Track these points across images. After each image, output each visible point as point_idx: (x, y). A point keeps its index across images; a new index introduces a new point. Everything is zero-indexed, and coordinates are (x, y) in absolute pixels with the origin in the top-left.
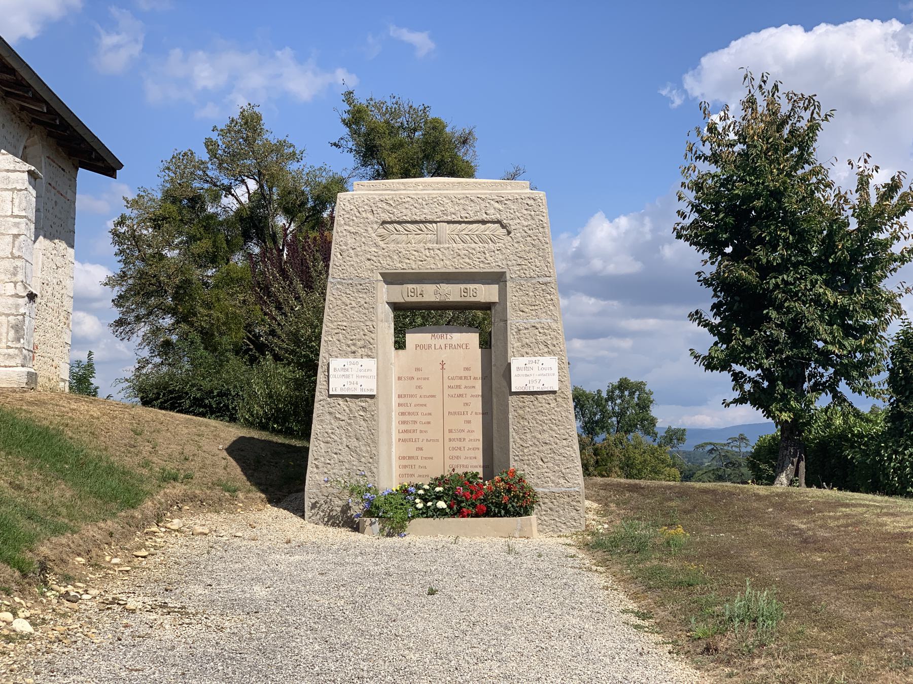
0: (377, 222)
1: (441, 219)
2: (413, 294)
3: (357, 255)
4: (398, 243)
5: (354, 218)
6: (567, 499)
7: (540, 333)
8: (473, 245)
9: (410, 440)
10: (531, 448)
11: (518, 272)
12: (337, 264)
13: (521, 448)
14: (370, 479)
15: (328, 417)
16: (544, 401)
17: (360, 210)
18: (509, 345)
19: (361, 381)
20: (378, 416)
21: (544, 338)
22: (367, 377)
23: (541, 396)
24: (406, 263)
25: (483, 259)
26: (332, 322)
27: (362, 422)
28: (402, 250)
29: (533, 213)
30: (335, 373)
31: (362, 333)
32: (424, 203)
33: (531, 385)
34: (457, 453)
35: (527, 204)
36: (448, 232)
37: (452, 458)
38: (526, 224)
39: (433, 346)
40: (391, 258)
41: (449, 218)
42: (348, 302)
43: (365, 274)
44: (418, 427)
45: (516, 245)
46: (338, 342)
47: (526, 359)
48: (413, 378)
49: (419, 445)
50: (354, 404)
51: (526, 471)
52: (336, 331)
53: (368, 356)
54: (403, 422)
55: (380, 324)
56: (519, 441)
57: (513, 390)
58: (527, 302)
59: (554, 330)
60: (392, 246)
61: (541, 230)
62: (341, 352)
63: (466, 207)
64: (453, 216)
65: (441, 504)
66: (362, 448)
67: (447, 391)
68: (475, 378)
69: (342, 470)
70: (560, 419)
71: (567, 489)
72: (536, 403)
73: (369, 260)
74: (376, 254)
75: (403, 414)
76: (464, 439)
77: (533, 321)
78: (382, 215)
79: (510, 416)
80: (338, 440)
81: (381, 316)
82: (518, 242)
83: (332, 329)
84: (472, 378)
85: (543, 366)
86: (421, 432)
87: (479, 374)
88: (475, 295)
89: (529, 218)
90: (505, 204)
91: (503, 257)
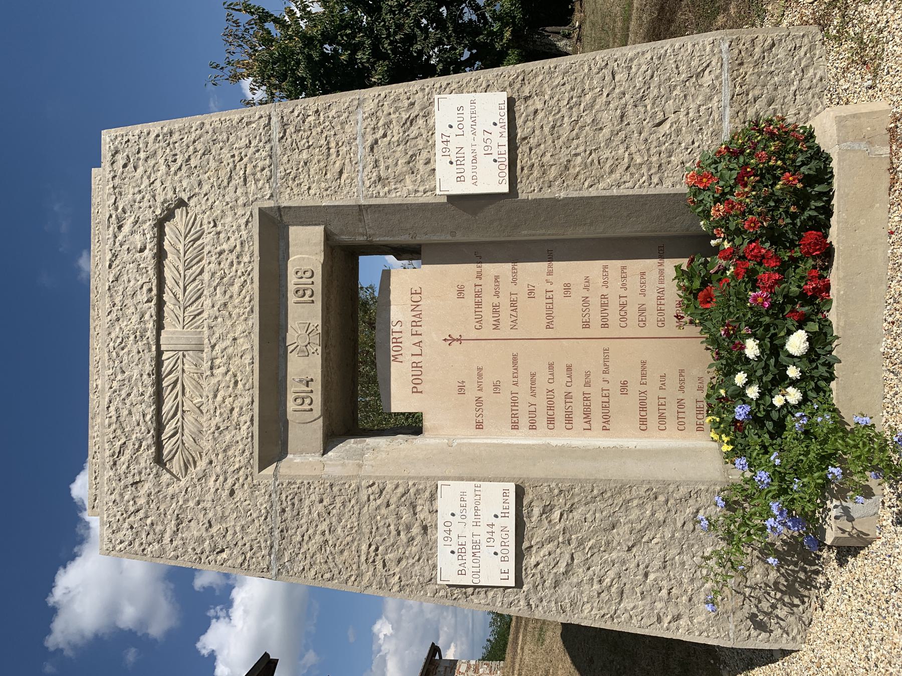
0: (157, 475)
1: (152, 342)
2: (307, 401)
3: (223, 518)
4: (200, 432)
5: (149, 521)
6: (748, 68)
7: (385, 136)
8: (206, 276)
9: (605, 406)
10: (633, 149)
11: (260, 184)
12: (240, 560)
13: (632, 169)
14: (702, 500)
15: (564, 589)
16: (530, 124)
17: (132, 509)
18: (411, 200)
19: (486, 517)
20: (562, 481)
21: (396, 128)
22: (477, 502)
23: (519, 131)
24: (240, 415)
25: (233, 257)
26: (360, 575)
27: (577, 515)
28: (213, 423)
29: (142, 155)
30: (469, 573)
31: (384, 511)
32: (119, 377)
33: (495, 151)
34: (632, 311)
35: (125, 166)
36: (179, 328)
37: (643, 323)
38: (163, 168)
39: (415, 359)
40: (228, 447)
41: (150, 325)
42: (318, 538)
43: (262, 501)
44: (577, 391)
45: (206, 188)
46: (404, 563)
47: (441, 164)
48: (479, 400)
49: (615, 389)
50: (536, 534)
51: (685, 156)
52: (380, 566)
53: (433, 498)
54: (569, 420)
55: (367, 470)
56: (616, 175)
57: (505, 188)
58: (322, 164)
59: (380, 105)
60: (206, 444)
61: (176, 137)
62: (424, 557)
63: (129, 291)
64: (147, 317)
65: (797, 343)
66: (633, 517)
67: (505, 331)
68: (479, 276)
69: (683, 564)
70: (568, 87)
71: (726, 67)
72: (533, 141)
73: (232, 493)
74: (221, 478)
75: (551, 420)
76: (604, 297)
77: (361, 150)
78: (143, 465)
79: (563, 195)
80: (616, 569)
81: (350, 469)
82: (200, 184)
83: (374, 575)
84: (478, 282)
85: (455, 125)
86: (587, 384)
87: (470, 269)
88: (308, 274)
89: (151, 162)
90: (124, 211)
91: (230, 213)
